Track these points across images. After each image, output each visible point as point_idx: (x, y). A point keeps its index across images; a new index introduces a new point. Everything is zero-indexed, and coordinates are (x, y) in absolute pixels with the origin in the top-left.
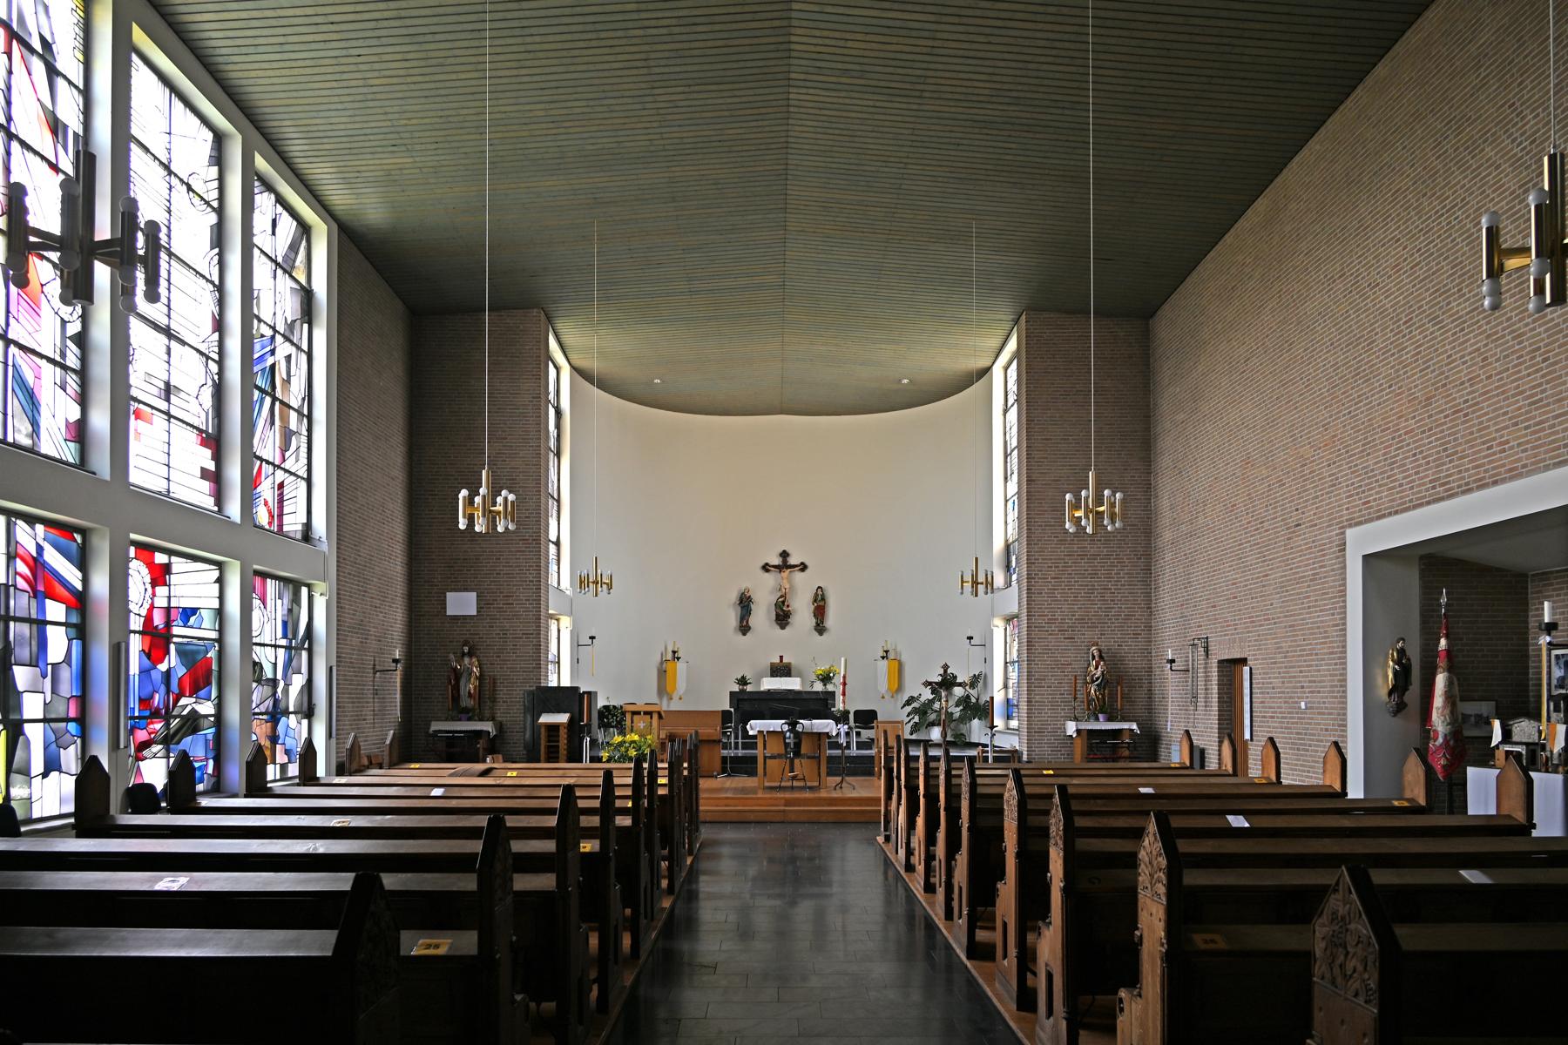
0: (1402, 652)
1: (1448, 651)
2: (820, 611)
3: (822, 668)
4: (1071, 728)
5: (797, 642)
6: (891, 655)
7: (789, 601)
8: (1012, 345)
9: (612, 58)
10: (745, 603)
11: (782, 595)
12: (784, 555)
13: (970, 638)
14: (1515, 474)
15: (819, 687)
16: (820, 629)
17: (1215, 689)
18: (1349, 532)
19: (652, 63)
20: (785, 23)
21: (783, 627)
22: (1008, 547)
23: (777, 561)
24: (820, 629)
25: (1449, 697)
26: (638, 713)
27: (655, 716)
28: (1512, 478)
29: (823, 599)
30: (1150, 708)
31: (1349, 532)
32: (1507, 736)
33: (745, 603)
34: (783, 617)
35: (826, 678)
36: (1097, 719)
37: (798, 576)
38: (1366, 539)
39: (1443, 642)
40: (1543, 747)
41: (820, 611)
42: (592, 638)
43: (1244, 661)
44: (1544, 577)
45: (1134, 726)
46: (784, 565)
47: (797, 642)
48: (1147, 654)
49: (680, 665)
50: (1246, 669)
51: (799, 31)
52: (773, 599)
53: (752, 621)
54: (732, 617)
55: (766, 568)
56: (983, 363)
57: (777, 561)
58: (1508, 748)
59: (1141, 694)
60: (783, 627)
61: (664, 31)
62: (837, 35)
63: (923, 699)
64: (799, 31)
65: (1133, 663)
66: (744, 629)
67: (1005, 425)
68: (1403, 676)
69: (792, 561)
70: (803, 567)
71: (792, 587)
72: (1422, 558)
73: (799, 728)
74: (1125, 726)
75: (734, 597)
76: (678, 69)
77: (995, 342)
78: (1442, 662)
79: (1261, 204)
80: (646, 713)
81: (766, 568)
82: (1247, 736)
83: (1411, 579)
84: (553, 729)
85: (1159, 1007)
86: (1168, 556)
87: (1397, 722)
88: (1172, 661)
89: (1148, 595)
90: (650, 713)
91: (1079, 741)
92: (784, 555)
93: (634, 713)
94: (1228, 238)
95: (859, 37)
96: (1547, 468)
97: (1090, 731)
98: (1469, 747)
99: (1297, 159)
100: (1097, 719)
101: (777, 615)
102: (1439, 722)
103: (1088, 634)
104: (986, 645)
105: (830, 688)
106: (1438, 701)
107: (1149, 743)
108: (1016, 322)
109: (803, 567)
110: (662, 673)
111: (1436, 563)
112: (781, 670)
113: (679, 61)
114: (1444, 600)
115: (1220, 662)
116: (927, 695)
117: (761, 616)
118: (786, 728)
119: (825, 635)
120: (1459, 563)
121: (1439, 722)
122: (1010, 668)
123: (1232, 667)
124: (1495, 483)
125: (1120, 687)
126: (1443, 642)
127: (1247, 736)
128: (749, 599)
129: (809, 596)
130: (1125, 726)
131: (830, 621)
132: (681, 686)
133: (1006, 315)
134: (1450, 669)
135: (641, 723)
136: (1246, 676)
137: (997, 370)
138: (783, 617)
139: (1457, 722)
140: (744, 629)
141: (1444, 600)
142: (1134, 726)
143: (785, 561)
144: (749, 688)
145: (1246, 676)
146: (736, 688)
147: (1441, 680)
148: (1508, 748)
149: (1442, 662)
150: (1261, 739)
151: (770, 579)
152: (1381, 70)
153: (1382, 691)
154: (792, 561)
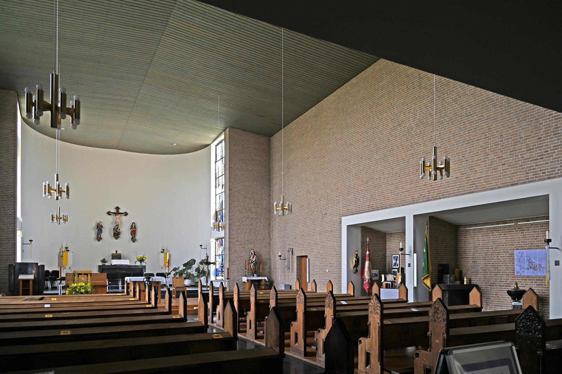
0: (357, 255)
1: (369, 255)
2: (133, 232)
3: (140, 256)
4: (245, 279)
5: (123, 244)
6: (165, 251)
7: (119, 228)
8: (222, 137)
9: (93, 7)
10: (99, 228)
11: (116, 224)
12: (117, 208)
13: (201, 246)
14: (391, 206)
15: (138, 264)
16: (134, 240)
17: (296, 266)
18: (342, 218)
19: (108, 13)
20: (168, 15)
21: (116, 239)
22: (216, 212)
23: (114, 211)
24: (134, 240)
25: (369, 268)
26: (81, 274)
27: (89, 276)
28: (390, 208)
29: (135, 228)
30: (270, 272)
31: (342, 218)
32: (385, 279)
33: (99, 228)
34: (117, 234)
35: (141, 260)
36: (254, 276)
37: (124, 218)
38: (348, 221)
39: (368, 252)
40: (395, 282)
41: (133, 232)
42: (31, 241)
43: (306, 257)
44: (391, 234)
45: (266, 278)
46: (117, 212)
47: (123, 244)
48: (269, 253)
49: (70, 254)
50: (308, 259)
51: (172, 19)
52: (113, 226)
53: (103, 235)
54: (93, 234)
55: (109, 213)
56: (208, 143)
57: (114, 211)
58: (386, 282)
59: (267, 267)
60: (116, 239)
61: (119, 5)
62: (187, 24)
63: (180, 269)
64: (172, 19)
65: (265, 257)
66: (99, 239)
67: (218, 167)
68: (357, 262)
69: (121, 211)
70: (126, 214)
71: (121, 222)
72: (362, 227)
73: (151, 280)
74: (263, 278)
75: (94, 225)
76: (119, 18)
77: (214, 136)
78: (367, 258)
79: (313, 109)
80: (84, 274)
81: (109, 213)
82: (308, 281)
83: (358, 233)
84: (26, 282)
85: (377, 338)
86: (277, 220)
87: (355, 275)
88: (280, 256)
89: (269, 233)
90: (87, 274)
91: (248, 284)
92: (117, 208)
93: (79, 274)
94: (302, 117)
95: (195, 27)
96: (399, 206)
97: (252, 280)
98: (375, 281)
99: (326, 99)
100: (254, 276)
101: (114, 233)
102: (367, 276)
103: (250, 246)
104: (207, 248)
105: (143, 264)
106: (366, 269)
107: (270, 284)
108: (224, 130)
109: (126, 214)
110: (61, 257)
111: (366, 229)
112: (117, 256)
113: (121, 16)
114: (368, 240)
115: (297, 257)
116: (182, 268)
117: (107, 234)
118: (145, 280)
119: (136, 243)
120: (377, 232)
121: (367, 276)
122: (217, 257)
123: (301, 258)
124: (386, 208)
125: (259, 265)
126: (368, 252)
127: (308, 281)
128: (101, 226)
129: (129, 226)
130: (263, 278)
131: (138, 237)
132: (70, 262)
133: (220, 126)
134: (370, 260)
135: (83, 278)
136: (308, 261)
137: (213, 146)
138: (117, 234)
139: (371, 276)
140: (99, 239)
141: (368, 240)
142: (266, 278)
143: (118, 211)
144: (107, 264)
145: (308, 261)
146: (101, 264)
147: (367, 263)
148: (386, 282)
149: (367, 258)
150: (312, 280)
151: (111, 218)
152: (354, 80)
153: (352, 266)
154: (121, 211)
